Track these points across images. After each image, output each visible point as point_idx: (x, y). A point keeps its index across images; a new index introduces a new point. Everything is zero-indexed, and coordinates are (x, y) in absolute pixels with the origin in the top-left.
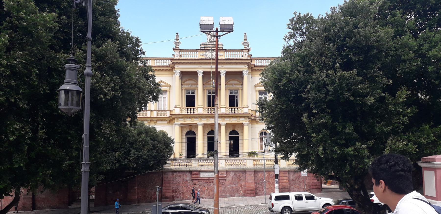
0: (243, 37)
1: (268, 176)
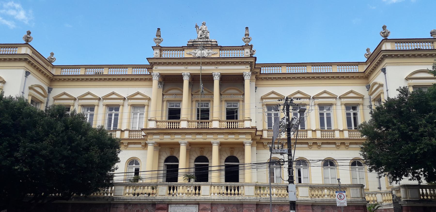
0: (244, 32)
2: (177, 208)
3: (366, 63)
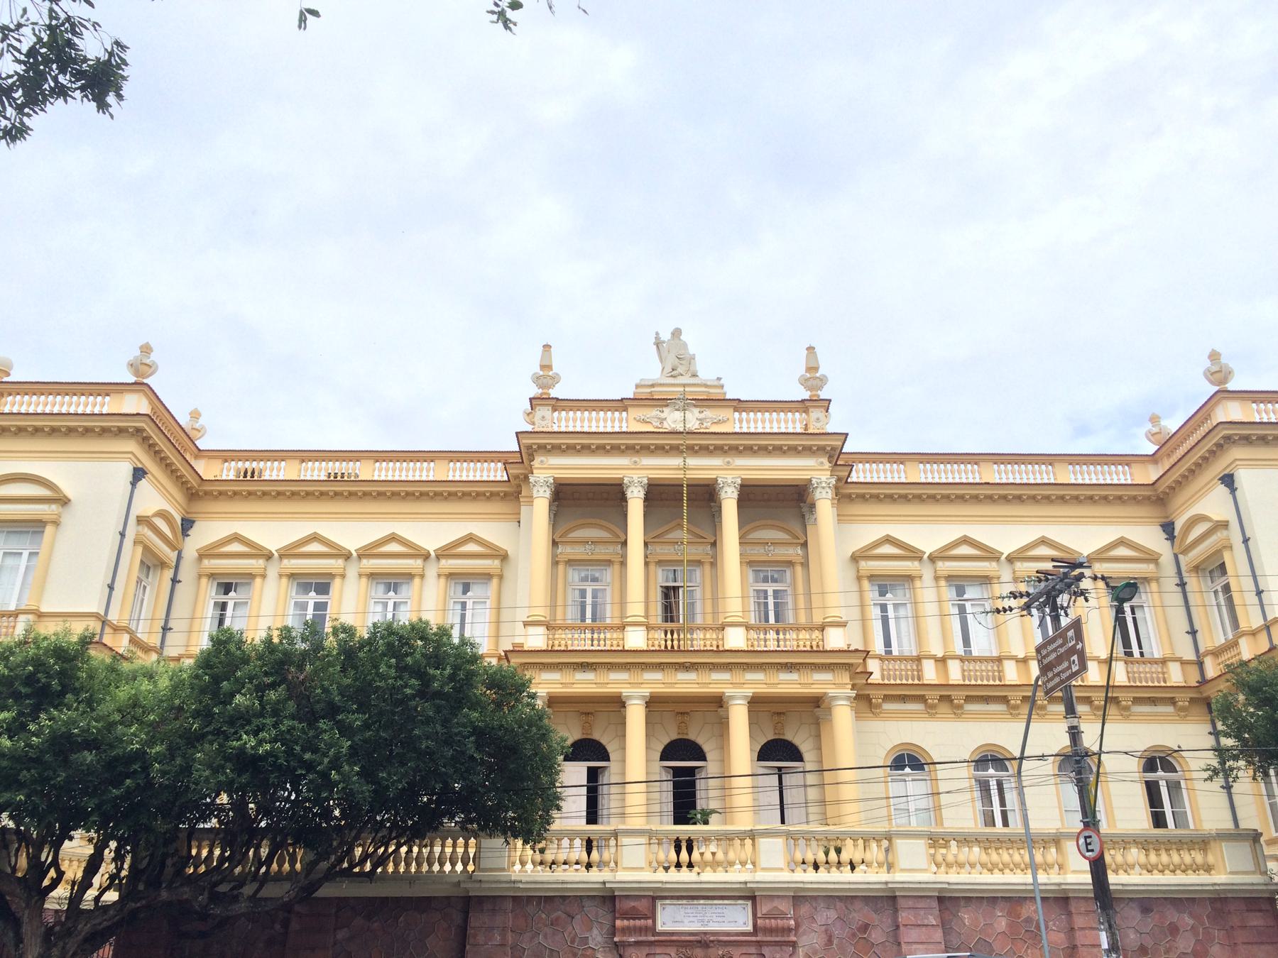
1: (1011, 925)
2: (682, 911)
3: (1153, 459)
